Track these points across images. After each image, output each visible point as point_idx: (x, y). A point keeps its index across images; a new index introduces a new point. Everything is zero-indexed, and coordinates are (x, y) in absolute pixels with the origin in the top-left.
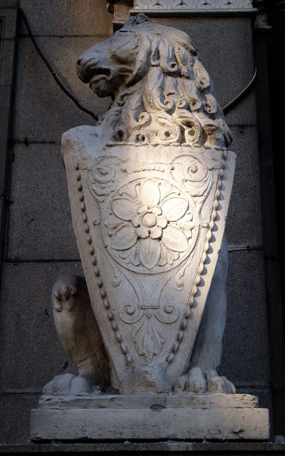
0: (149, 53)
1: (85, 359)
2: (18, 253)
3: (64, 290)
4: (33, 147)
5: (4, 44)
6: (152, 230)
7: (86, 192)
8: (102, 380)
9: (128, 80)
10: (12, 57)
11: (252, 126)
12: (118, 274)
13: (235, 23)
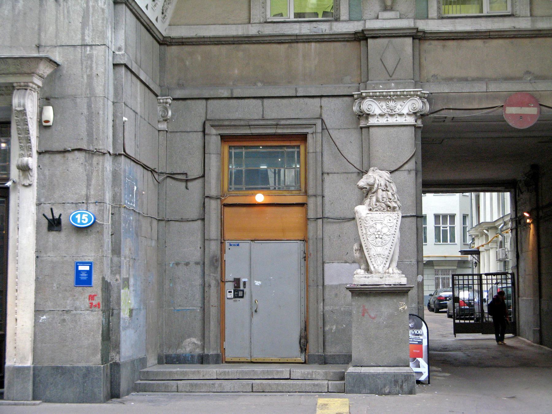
0: (378, 185)
4: (331, 175)
7: (362, 225)
8: (368, 270)
13: (408, 128)
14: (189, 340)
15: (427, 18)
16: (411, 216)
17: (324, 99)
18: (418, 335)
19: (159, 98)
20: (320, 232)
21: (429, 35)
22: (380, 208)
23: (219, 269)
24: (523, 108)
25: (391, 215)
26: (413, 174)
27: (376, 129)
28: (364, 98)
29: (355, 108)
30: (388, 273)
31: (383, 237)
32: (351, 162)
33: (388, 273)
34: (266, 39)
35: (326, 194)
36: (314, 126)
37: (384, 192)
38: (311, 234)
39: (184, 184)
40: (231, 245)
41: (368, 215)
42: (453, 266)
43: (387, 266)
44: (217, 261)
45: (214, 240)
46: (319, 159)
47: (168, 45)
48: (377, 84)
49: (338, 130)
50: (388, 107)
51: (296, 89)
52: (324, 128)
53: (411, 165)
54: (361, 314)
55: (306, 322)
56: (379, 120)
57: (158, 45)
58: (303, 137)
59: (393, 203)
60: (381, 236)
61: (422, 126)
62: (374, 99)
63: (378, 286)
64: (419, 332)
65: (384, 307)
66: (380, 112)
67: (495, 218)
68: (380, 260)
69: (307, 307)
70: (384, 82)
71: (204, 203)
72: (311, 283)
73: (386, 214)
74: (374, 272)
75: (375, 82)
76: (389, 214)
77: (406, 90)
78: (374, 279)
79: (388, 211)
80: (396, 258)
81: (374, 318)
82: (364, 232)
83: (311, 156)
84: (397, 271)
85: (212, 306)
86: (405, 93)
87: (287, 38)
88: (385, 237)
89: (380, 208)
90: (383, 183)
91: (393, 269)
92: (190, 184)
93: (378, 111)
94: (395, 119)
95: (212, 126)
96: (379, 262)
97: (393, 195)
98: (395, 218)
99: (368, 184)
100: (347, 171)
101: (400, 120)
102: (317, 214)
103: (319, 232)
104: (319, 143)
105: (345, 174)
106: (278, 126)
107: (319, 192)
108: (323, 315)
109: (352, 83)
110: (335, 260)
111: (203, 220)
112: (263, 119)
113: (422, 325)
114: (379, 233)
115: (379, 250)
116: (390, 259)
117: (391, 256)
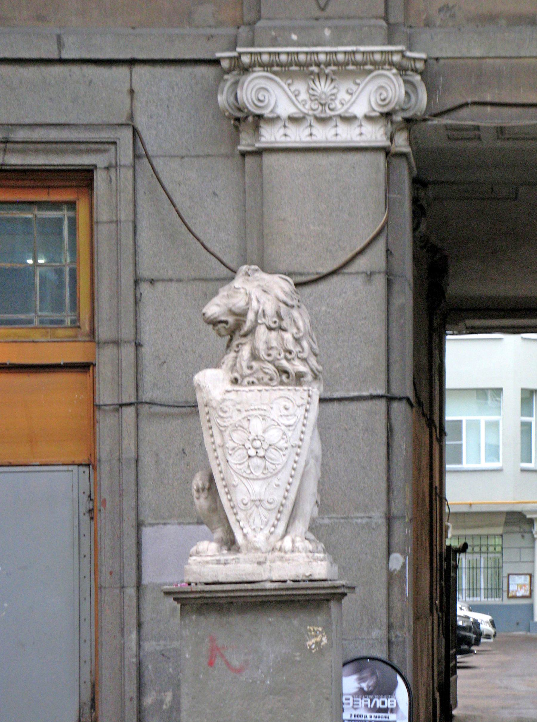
0: (257, 314)
1: (263, 242)
2: (152, 396)
3: (200, 485)
4: (160, 286)
5: (121, 172)
6: (258, 451)
7: (213, 423)
11: (379, 272)
12: (236, 479)
13: (368, 157)
16: (373, 397)
17: (139, 70)
18: (385, 711)
20: (129, 443)
22: (261, 375)
25: (290, 394)
27: (281, 158)
28: (246, 70)
29: (222, 99)
30: (280, 550)
31: (269, 454)
32: (216, 250)
33: (280, 550)
35: (145, 338)
36: (112, 147)
37: (274, 334)
38: (105, 449)
41: (228, 396)
42: (492, 525)
43: (281, 529)
46: (127, 240)
48: (283, 29)
49: (178, 160)
50: (313, 97)
51: (59, 37)
53: (375, 259)
54: (204, 661)
55: (93, 685)
56: (288, 132)
58: (83, 178)
59: (297, 362)
60: (261, 453)
62: (275, 73)
64: (388, 704)
65: (268, 640)
68: (259, 516)
69: (97, 645)
70: (304, 23)
72: (106, 580)
73: (278, 394)
74: (243, 549)
75: (277, 23)
76: (284, 391)
77: (362, 48)
78: (241, 566)
79: (282, 383)
80: (309, 508)
81: (239, 671)
82: (218, 440)
83: (103, 232)
86: (359, 57)
89: (261, 375)
90: (270, 308)
91: (298, 540)
93: (285, 109)
94: (333, 132)
96: (258, 521)
97: (297, 340)
98: (299, 402)
99: (232, 312)
100: (203, 275)
101: (347, 135)
102: (120, 394)
103: (125, 442)
104: (127, 196)
105: (201, 284)
106: (9, 145)
107: (127, 333)
108: (139, 665)
109: (220, 24)
110: (170, 517)
113: (395, 685)
114: (257, 444)
115: (258, 489)
116: (287, 511)
117: (289, 504)
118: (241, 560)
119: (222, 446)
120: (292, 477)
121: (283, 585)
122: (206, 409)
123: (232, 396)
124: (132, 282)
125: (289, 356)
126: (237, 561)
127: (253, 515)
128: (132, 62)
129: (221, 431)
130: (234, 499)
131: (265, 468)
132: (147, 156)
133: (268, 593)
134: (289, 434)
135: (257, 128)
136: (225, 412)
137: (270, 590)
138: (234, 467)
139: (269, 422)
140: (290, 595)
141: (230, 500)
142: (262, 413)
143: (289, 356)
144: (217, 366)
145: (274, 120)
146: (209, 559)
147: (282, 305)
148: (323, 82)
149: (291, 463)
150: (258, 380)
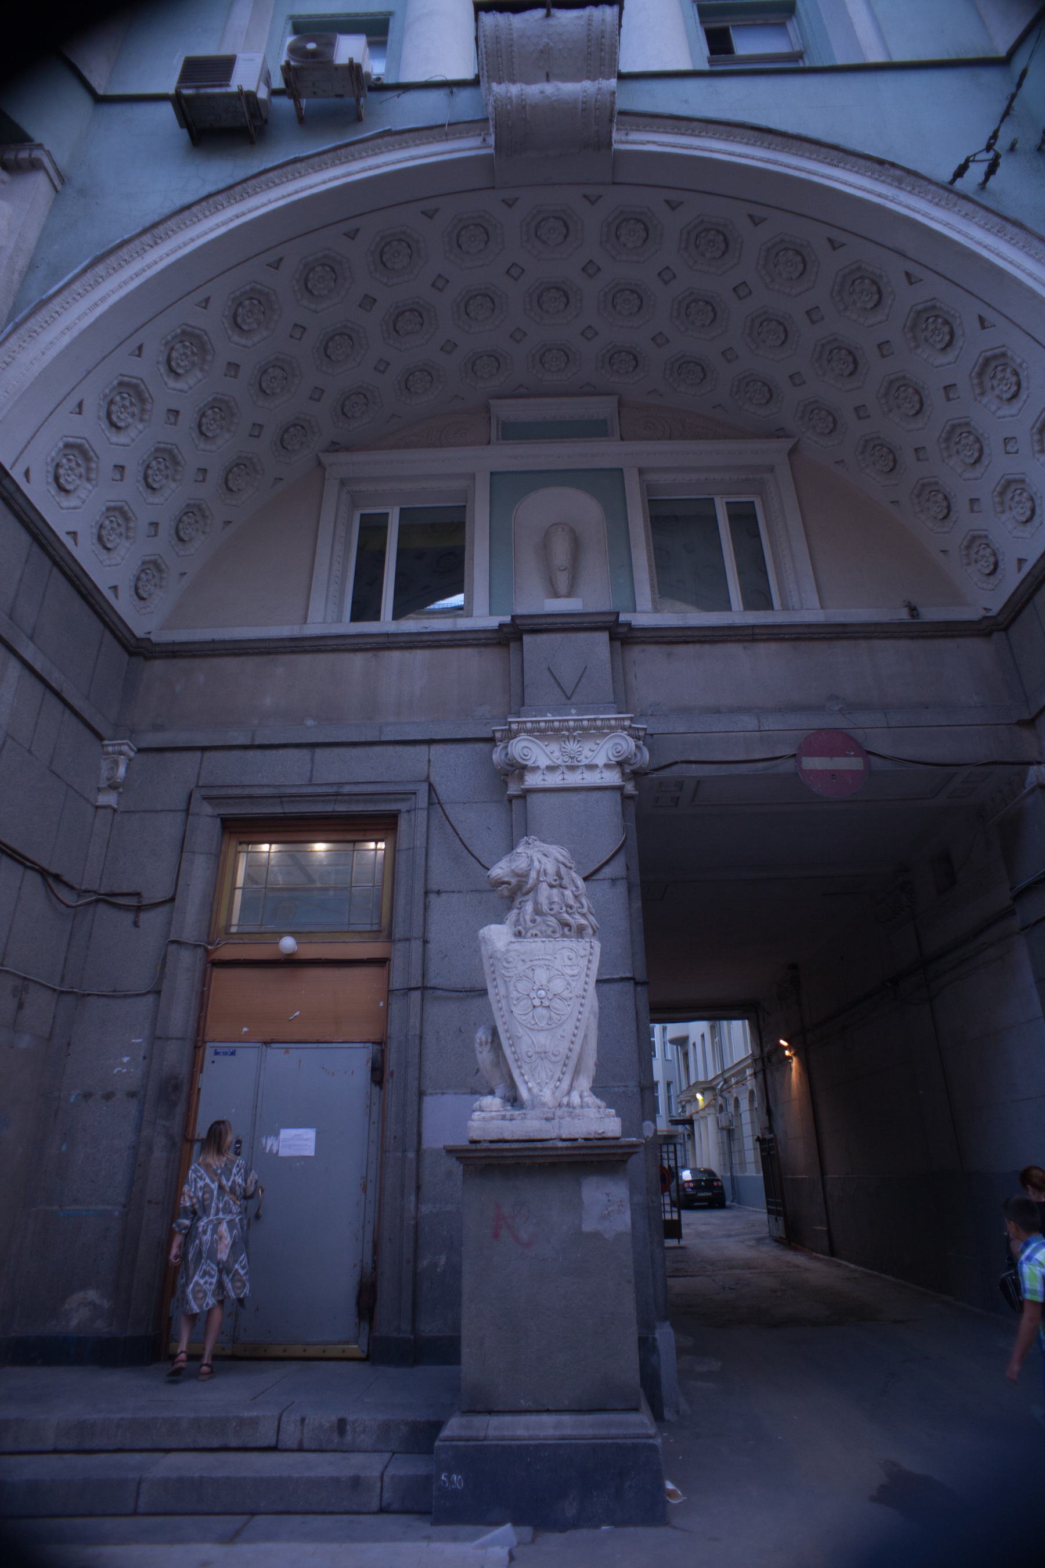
0: (539, 872)
4: (444, 896)
9: (524, 890)
10: (425, 823)
13: (608, 793)
14: (81, 1294)
15: (635, 611)
16: (622, 979)
17: (435, 749)
19: (106, 742)
21: (639, 635)
22: (544, 928)
23: (180, 1109)
24: (835, 759)
26: (621, 888)
27: (540, 795)
33: (568, 1105)
34: (329, 642)
36: (413, 797)
37: (555, 891)
39: (130, 917)
40: (217, 1053)
41: (512, 945)
43: (565, 1085)
44: (177, 1088)
45: (178, 1039)
47: (147, 658)
50: (563, 753)
52: (434, 800)
56: (546, 777)
57: (126, 656)
59: (577, 916)
60: (546, 1003)
61: (636, 793)
62: (536, 737)
63: (539, 1145)
66: (549, 763)
67: (711, 1076)
71: (165, 957)
79: (564, 935)
84: (591, 1099)
85: (150, 1202)
87: (370, 640)
88: (557, 1004)
90: (551, 868)
92: (144, 917)
93: (543, 762)
94: (580, 777)
95: (205, 798)
97: (576, 897)
98: (582, 953)
101: (592, 778)
108: (417, 1225)
111: (158, 993)
112: (311, 784)
114: (542, 993)
115: (542, 1039)
116: (572, 1064)
117: (574, 1056)
118: (528, 1116)
119: (507, 997)
120: (577, 1028)
121: (575, 1144)
122: (491, 961)
123: (516, 946)
124: (422, 893)
125: (570, 911)
126: (524, 1117)
127: (539, 1068)
128: (430, 742)
129: (505, 982)
130: (518, 1051)
131: (550, 1018)
132: (439, 803)
133: (560, 1152)
134: (574, 984)
135: (521, 778)
136: (509, 962)
137: (562, 1148)
138: (519, 1018)
139: (554, 972)
140: (584, 1155)
141: (514, 1053)
142: (547, 963)
143: (570, 911)
144: (501, 921)
145: (535, 769)
146: (494, 1114)
147: (561, 866)
148: (572, 742)
149: (576, 1014)
150: (541, 932)
